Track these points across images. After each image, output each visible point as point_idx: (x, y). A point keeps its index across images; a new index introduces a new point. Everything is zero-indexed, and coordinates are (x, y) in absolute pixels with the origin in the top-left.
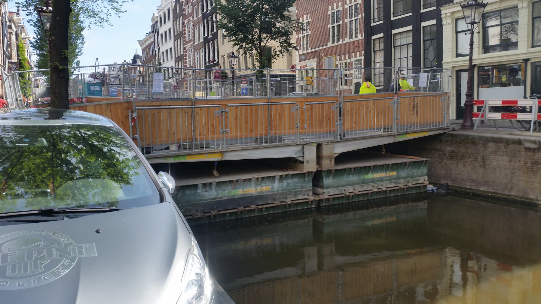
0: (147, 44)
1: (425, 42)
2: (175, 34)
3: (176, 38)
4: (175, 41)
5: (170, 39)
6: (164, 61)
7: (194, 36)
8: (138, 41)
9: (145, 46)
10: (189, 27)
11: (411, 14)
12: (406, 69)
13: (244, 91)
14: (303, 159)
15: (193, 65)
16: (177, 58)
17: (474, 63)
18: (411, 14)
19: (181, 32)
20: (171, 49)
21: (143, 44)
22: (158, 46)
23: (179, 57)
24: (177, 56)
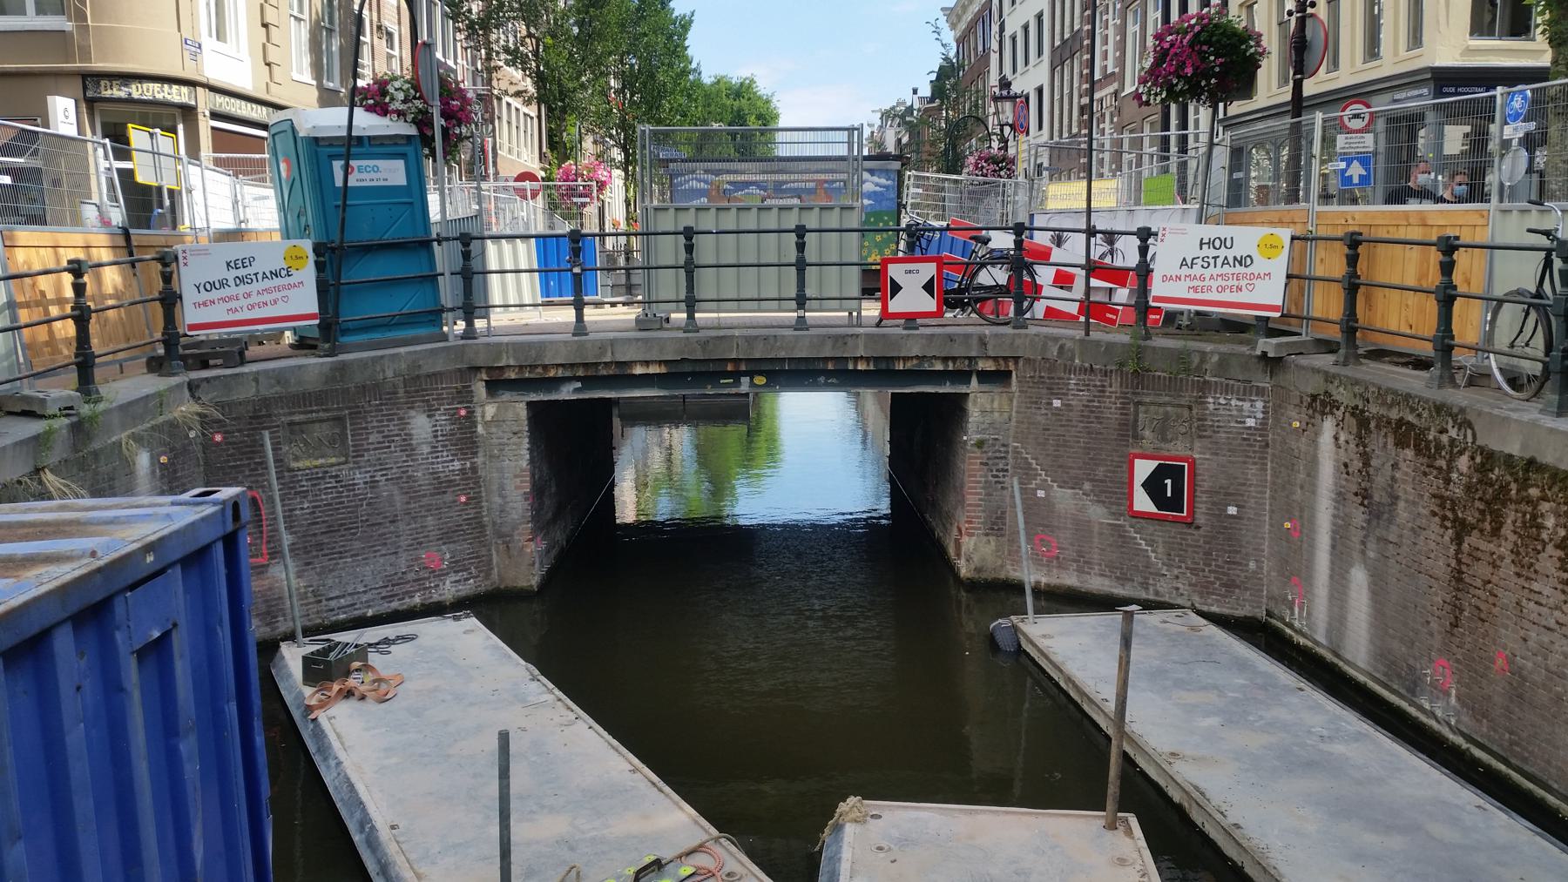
0: (969, 17)
1: (80, 81)
2: (1057, 43)
3: (1061, 57)
4: (1053, 70)
5: (1040, 53)
6: (1014, 71)
7: (1121, 62)
8: (942, 9)
9: (963, 26)
10: (1104, 129)
11: (1169, 494)
12: (156, 150)
13: (1356, 170)
14: (214, 542)
15: (1117, 70)
16: (1059, 51)
17: (354, 134)
18: (1169, 494)
19: (1075, 35)
20: (1040, 91)
21: (959, 18)
22: (1001, 16)
23: (1064, 42)
24: (1057, 43)
